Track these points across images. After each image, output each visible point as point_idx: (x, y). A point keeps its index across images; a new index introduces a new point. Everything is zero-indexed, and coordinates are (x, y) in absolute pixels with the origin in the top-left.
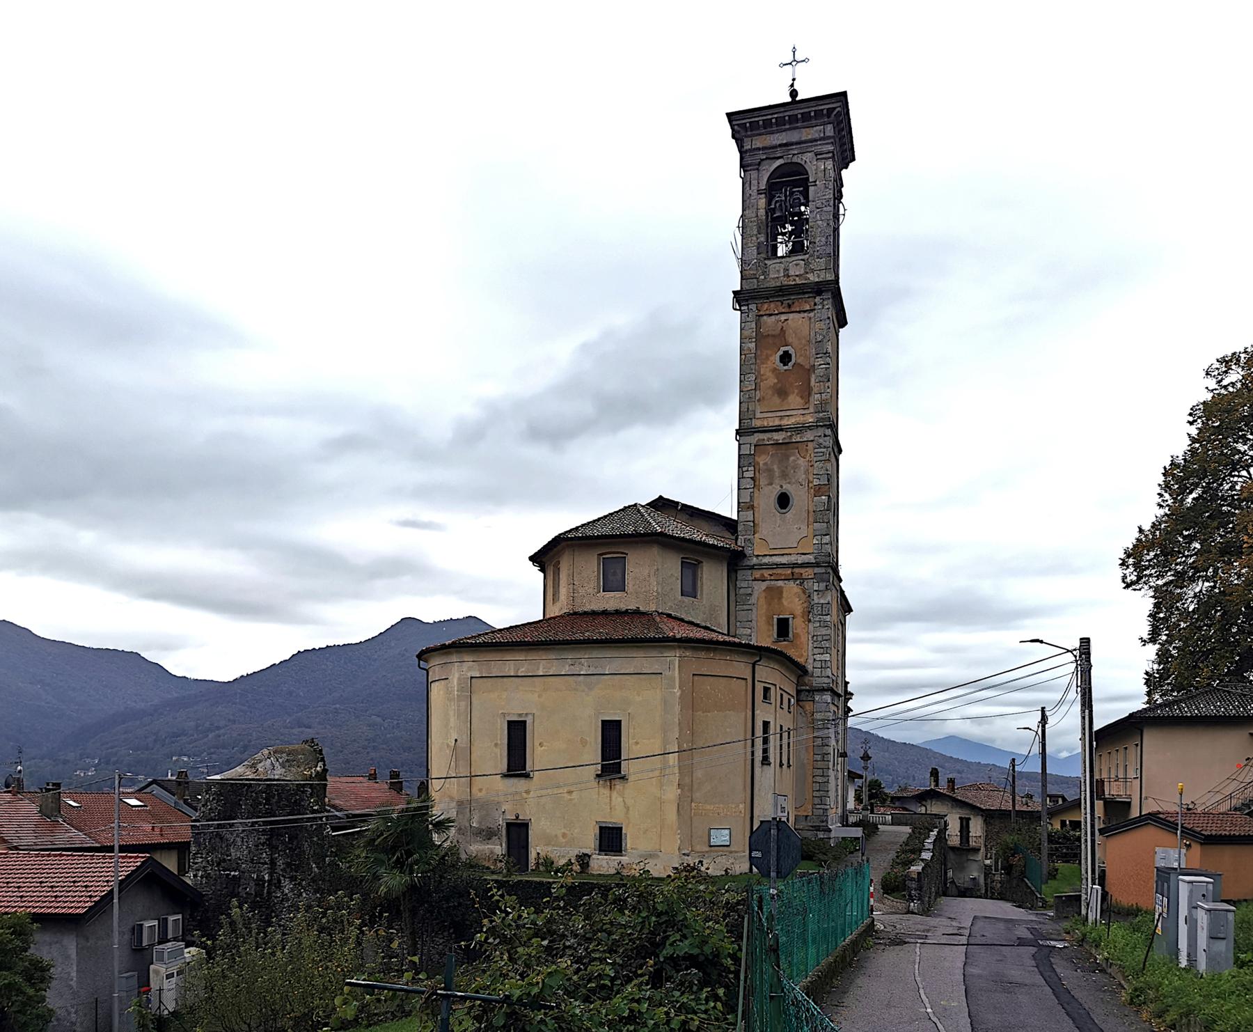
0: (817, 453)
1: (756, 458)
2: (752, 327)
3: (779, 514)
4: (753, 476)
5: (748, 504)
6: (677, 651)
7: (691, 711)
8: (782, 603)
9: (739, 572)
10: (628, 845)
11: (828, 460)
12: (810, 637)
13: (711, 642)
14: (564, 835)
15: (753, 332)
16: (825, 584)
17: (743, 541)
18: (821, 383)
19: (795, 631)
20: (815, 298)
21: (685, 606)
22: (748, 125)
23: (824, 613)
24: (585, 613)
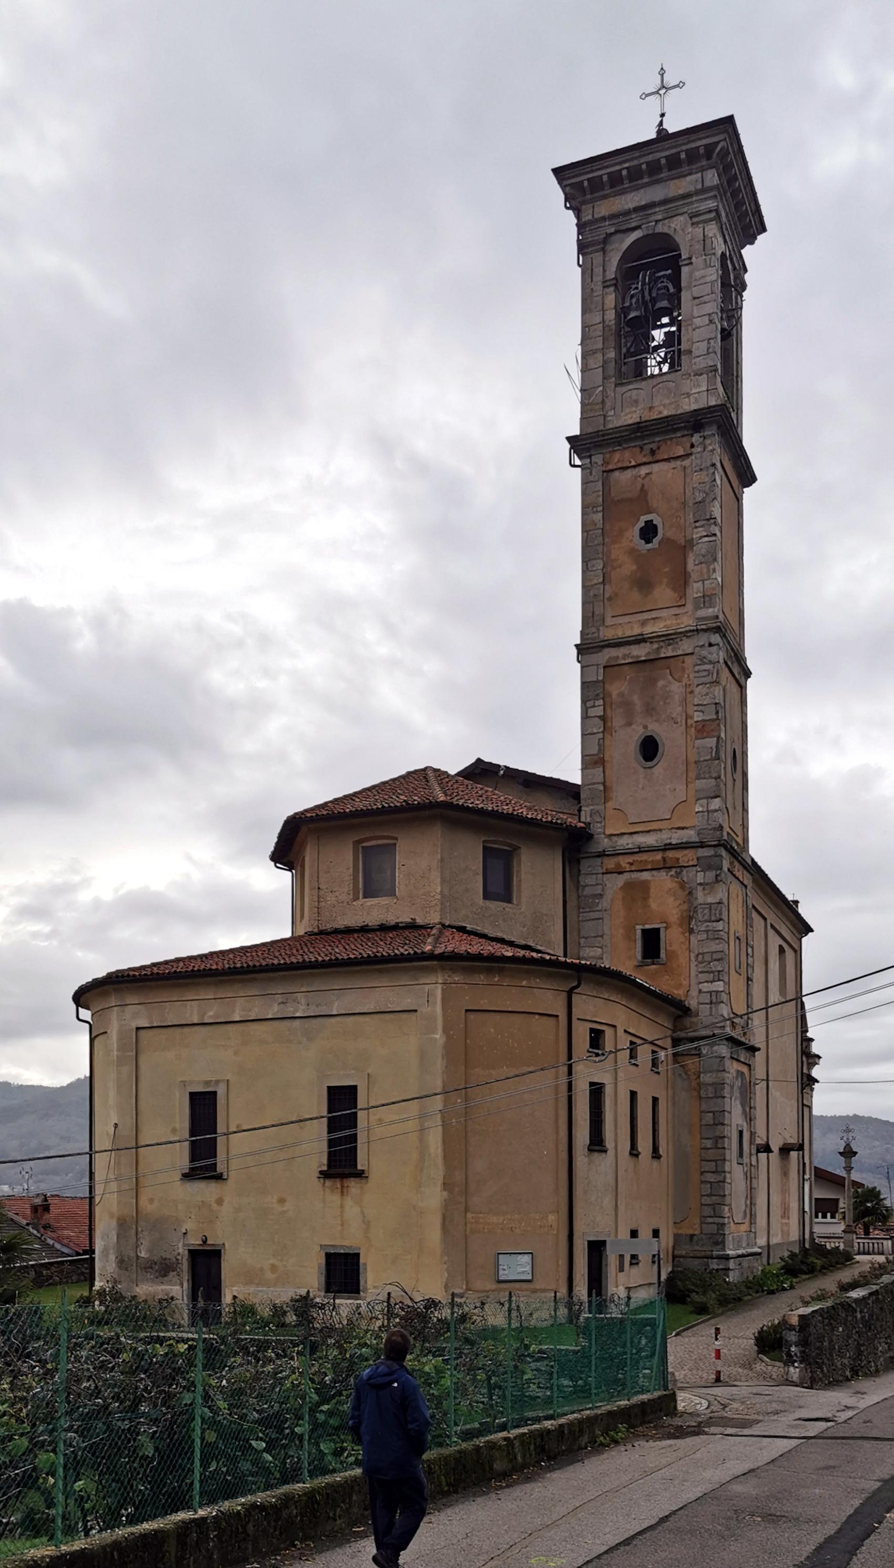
0: (698, 672)
1: (607, 686)
2: (597, 489)
3: (642, 770)
4: (602, 714)
5: (596, 757)
6: (440, 975)
7: (463, 1067)
8: (649, 906)
9: (582, 864)
10: (369, 1282)
11: (715, 681)
12: (693, 956)
13: (492, 958)
14: (273, 1268)
15: (598, 496)
16: (714, 873)
17: (588, 814)
18: (703, 565)
19: (668, 948)
20: (692, 436)
21: (491, 916)
22: (586, 183)
23: (713, 918)
24: (336, 931)
